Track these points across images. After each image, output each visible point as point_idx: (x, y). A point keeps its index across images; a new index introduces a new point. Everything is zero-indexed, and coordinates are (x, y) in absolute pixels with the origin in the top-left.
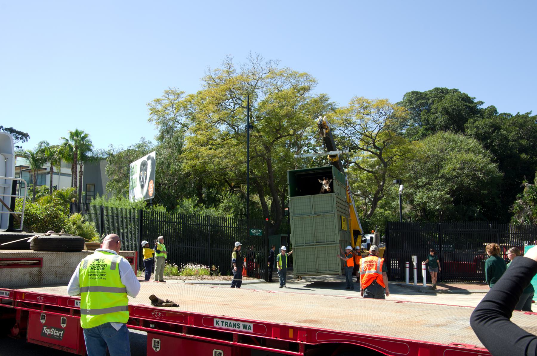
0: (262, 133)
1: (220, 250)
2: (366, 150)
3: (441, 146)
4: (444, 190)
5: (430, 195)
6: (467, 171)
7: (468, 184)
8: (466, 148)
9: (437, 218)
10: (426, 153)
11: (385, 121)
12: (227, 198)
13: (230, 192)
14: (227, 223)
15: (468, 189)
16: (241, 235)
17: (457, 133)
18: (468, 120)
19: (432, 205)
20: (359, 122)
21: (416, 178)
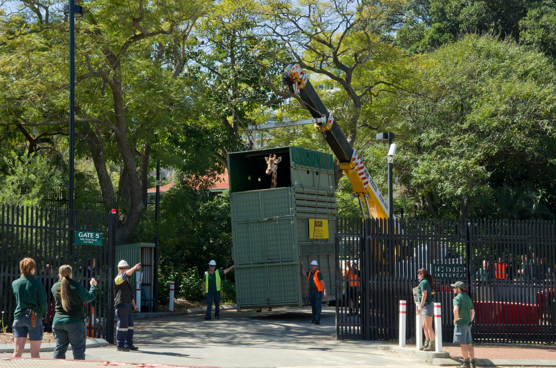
0: (102, 26)
1: (7, 277)
2: (318, 72)
3: (470, 66)
4: (472, 157)
5: (444, 166)
6: (521, 119)
7: (522, 144)
8: (520, 70)
9: (456, 212)
10: (439, 80)
11: (360, 10)
12: (23, 162)
13: (30, 151)
14: (25, 217)
15: (522, 154)
16: (55, 243)
17: (503, 40)
18: (526, 12)
19: (448, 187)
20: (305, 10)
21: (416, 131)
